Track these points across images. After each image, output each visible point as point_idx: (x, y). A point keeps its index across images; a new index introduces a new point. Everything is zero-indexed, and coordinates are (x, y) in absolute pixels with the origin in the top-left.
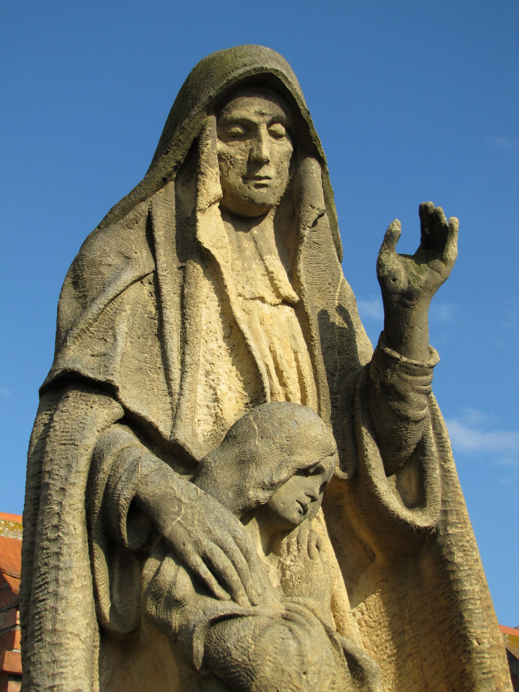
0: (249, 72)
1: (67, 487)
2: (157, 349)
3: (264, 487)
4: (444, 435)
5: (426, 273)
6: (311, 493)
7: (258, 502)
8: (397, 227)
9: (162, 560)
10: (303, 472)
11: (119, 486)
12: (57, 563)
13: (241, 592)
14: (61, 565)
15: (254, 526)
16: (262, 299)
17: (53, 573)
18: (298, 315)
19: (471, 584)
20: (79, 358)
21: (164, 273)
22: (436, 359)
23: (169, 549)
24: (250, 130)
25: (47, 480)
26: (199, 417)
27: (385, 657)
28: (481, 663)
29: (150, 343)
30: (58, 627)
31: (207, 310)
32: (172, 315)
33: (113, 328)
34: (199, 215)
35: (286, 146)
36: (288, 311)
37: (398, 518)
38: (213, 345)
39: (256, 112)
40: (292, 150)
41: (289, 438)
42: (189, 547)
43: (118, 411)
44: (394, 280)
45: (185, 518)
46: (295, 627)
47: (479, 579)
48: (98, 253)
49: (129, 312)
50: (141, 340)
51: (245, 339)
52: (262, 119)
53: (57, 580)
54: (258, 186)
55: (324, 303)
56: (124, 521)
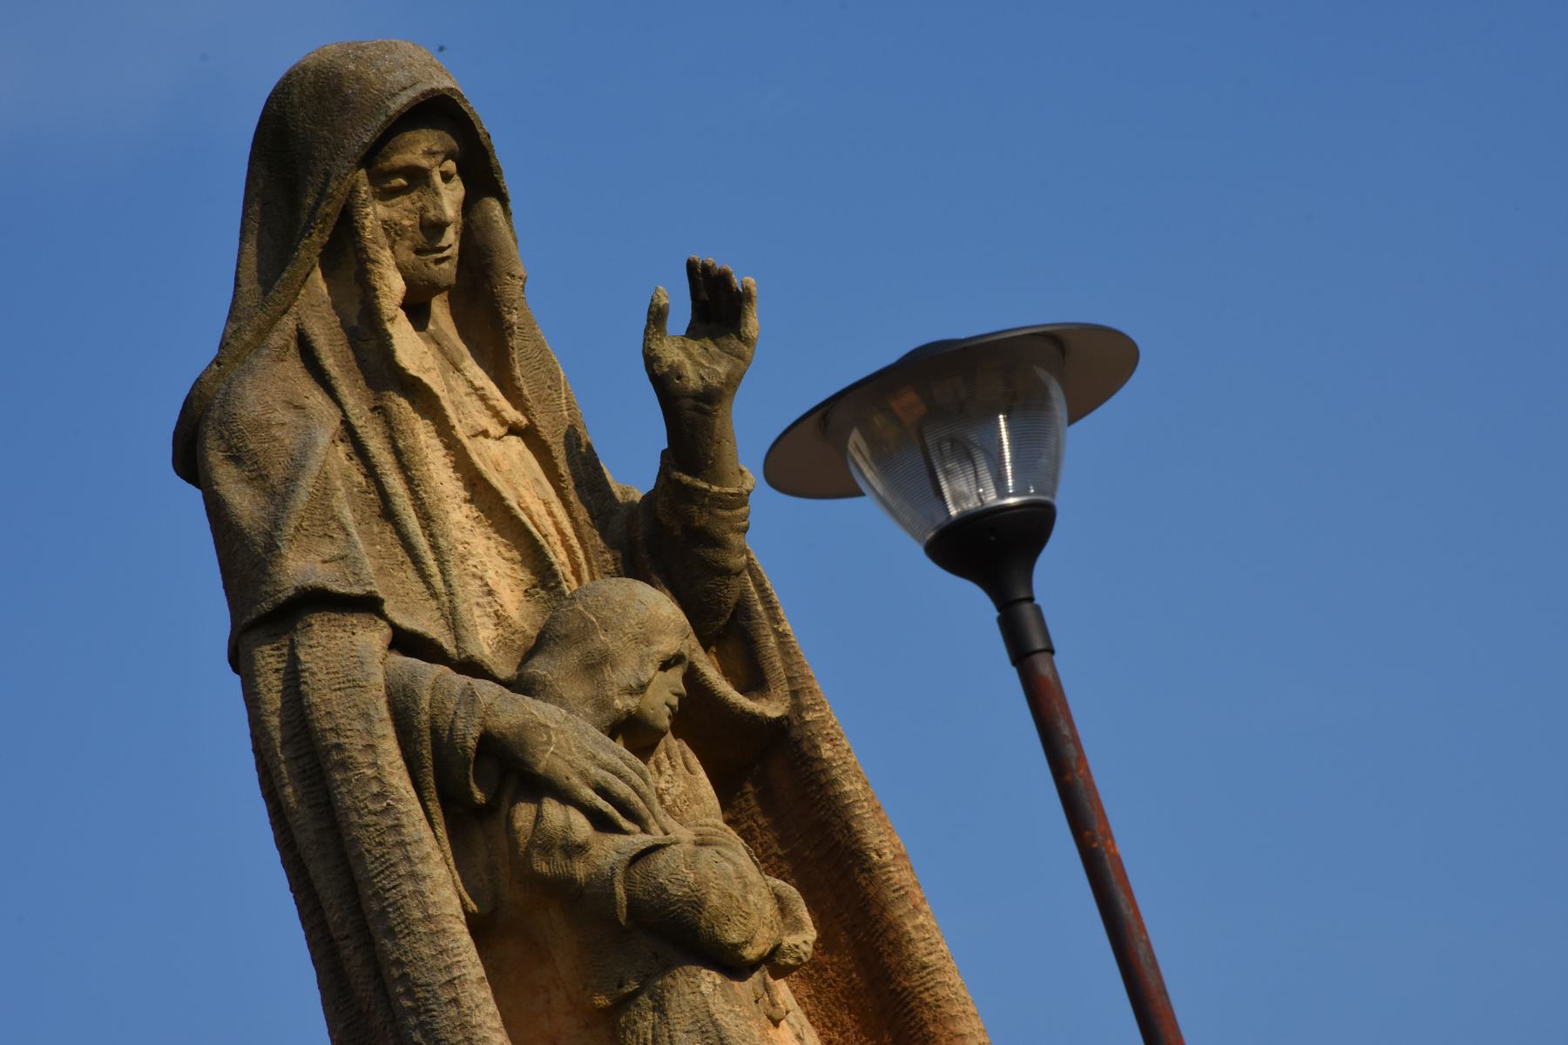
0: (416, 99)
1: (376, 742)
2: (389, 536)
3: (631, 692)
5: (724, 363)
9: (540, 803)
10: (665, 666)
11: (460, 724)
12: (398, 838)
13: (651, 820)
14: (407, 839)
16: (485, 434)
18: (529, 446)
23: (541, 787)
24: (417, 178)
28: (889, 879)
32: (395, 483)
33: (333, 518)
36: (516, 444)
41: (641, 624)
42: (575, 781)
44: (679, 378)
46: (723, 850)
47: (858, 774)
53: (408, 859)
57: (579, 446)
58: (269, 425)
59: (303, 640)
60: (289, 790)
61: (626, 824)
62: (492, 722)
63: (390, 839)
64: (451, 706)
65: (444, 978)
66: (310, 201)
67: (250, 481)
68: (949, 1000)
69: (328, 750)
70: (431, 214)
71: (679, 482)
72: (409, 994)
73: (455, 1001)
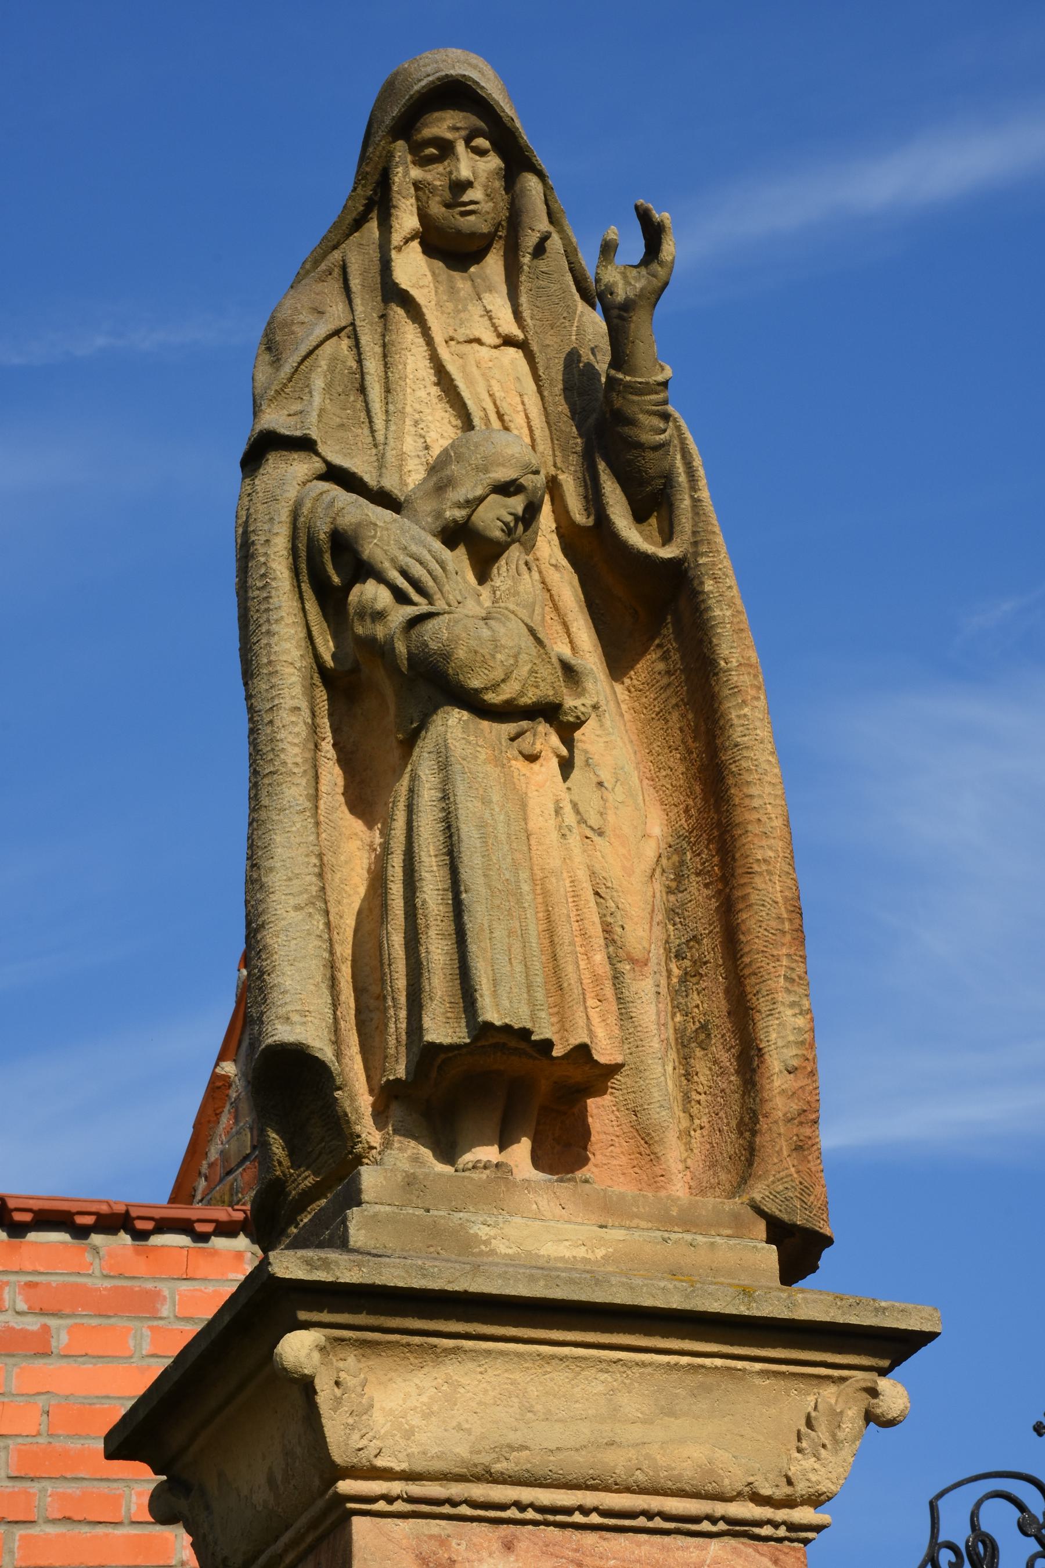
0: (433, 82)
2: (360, 405)
3: (459, 506)
4: (694, 464)
6: (513, 511)
7: (455, 521)
8: (612, 233)
13: (438, 596)
14: (271, 607)
15: (461, 551)
16: (478, 341)
17: (265, 616)
19: (721, 610)
20: (277, 419)
21: (363, 323)
22: (668, 373)
25: (253, 538)
26: (410, 468)
27: (653, 716)
29: (352, 398)
30: (273, 658)
31: (413, 358)
32: (373, 366)
34: (394, 254)
35: (493, 162)
36: (513, 354)
37: (638, 551)
38: (422, 393)
39: (449, 127)
40: (503, 166)
42: (387, 565)
43: (318, 466)
45: (381, 539)
48: (289, 312)
49: (325, 367)
50: (343, 397)
51: (452, 380)
52: (457, 135)
54: (464, 214)
55: (559, 341)
56: (327, 557)
57: (579, 361)
58: (293, 323)
68: (748, 770)
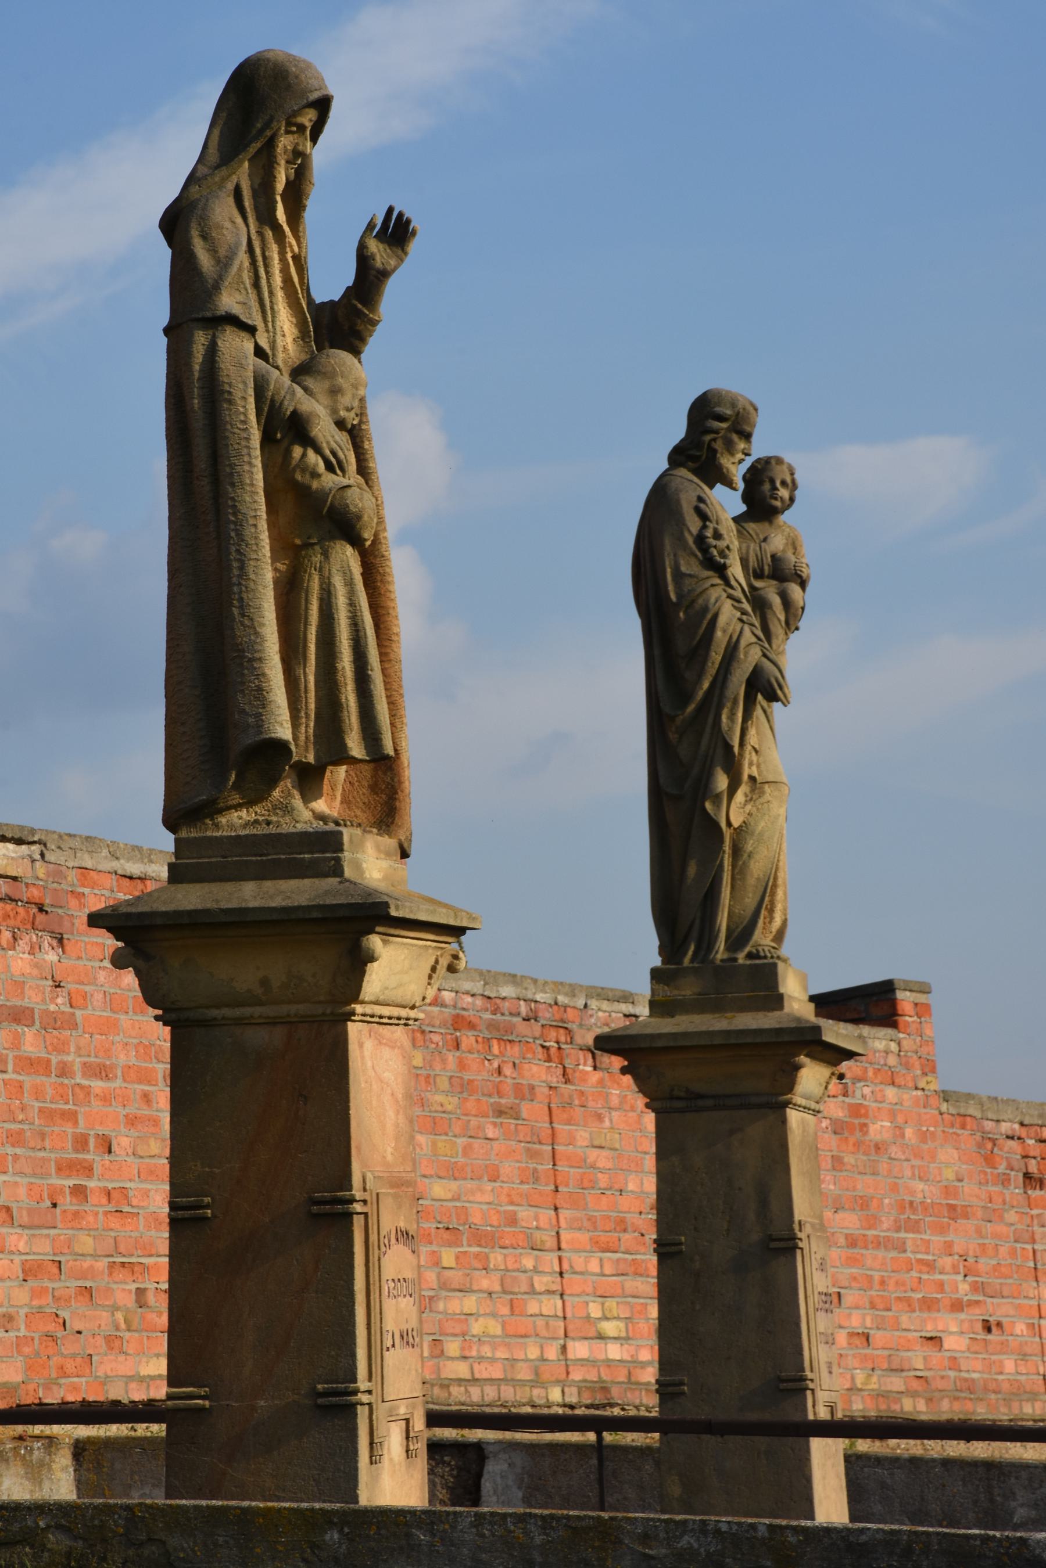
11: (286, 403)
23: (309, 442)
42: (324, 445)
53: (249, 455)
59: (221, 336)
60: (196, 401)
61: (338, 471)
62: (299, 406)
63: (244, 443)
64: (283, 393)
65: (253, 514)
66: (259, 125)
67: (208, 250)
69: (223, 392)
70: (300, 148)
71: (355, 306)
72: (235, 514)
73: (255, 526)
